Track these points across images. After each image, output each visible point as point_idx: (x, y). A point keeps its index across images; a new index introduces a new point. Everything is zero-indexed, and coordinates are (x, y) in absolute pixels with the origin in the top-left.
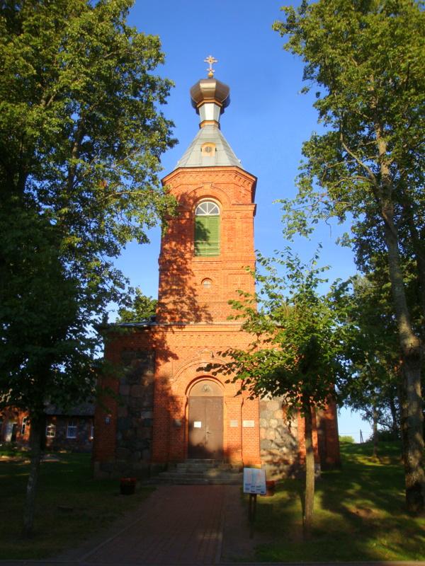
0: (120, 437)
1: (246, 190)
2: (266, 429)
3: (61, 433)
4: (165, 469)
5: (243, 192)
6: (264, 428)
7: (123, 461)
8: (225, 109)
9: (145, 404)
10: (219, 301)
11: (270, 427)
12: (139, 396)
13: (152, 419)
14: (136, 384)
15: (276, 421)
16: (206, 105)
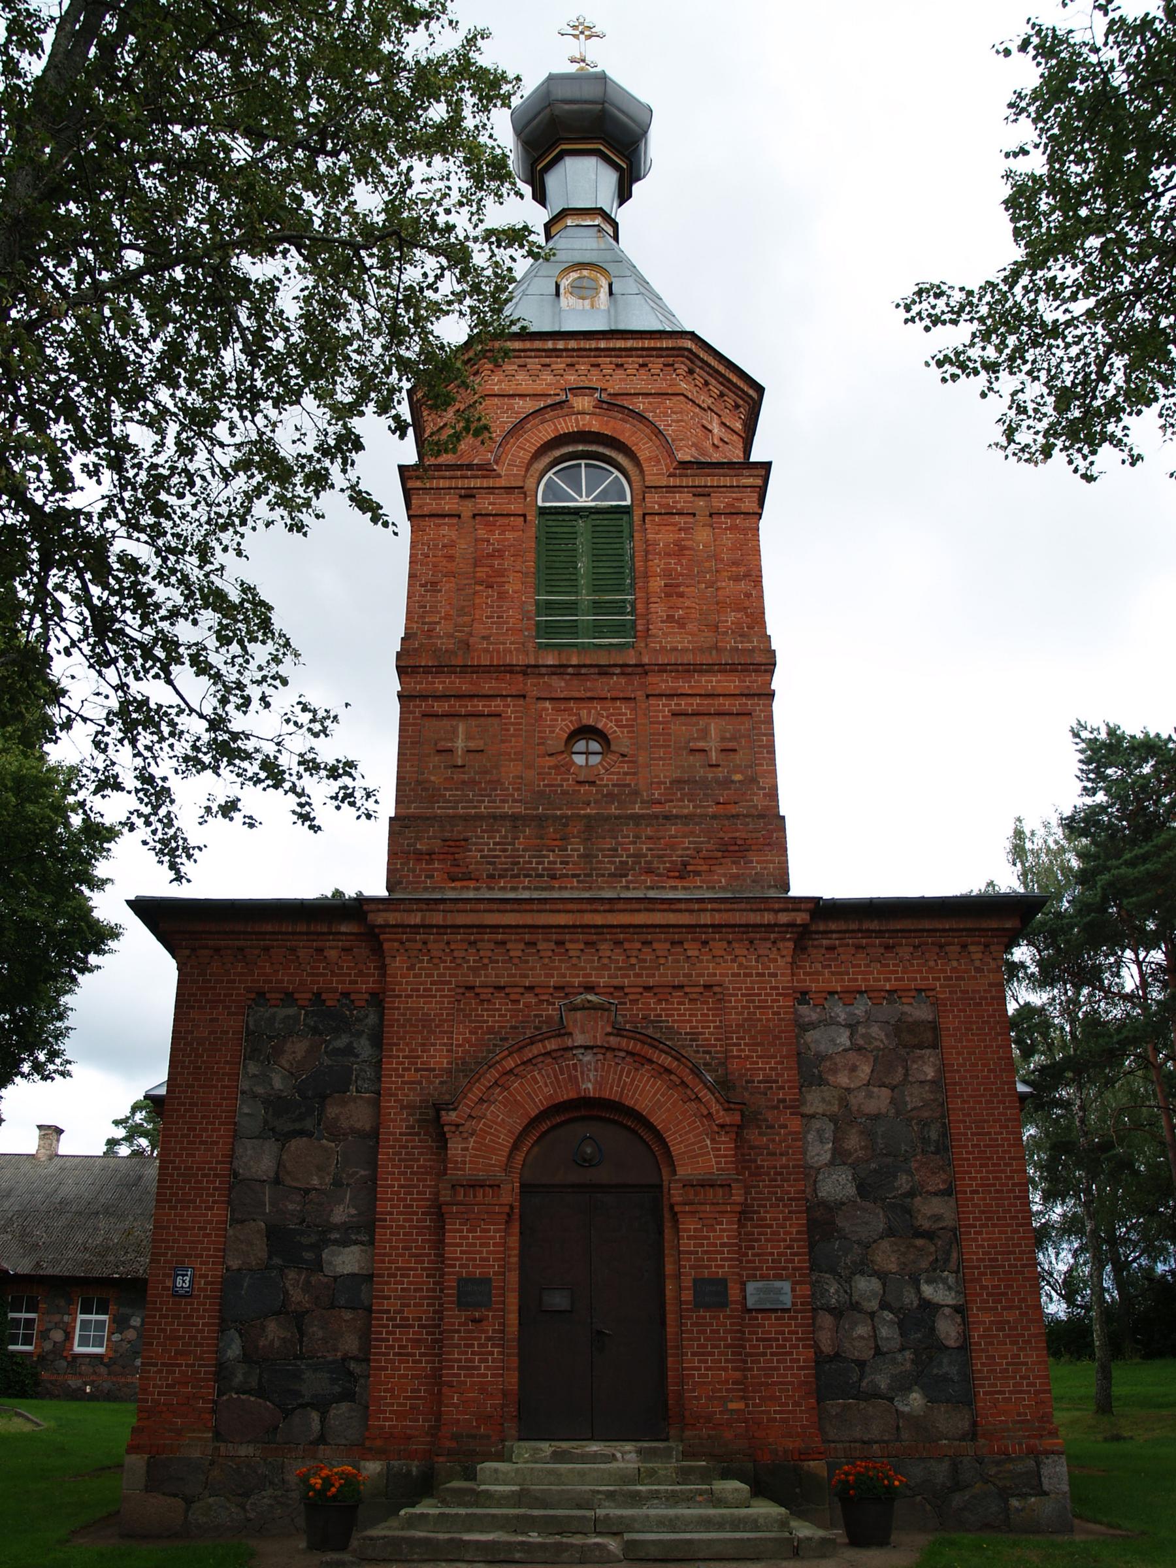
0: (234, 1351)
1: (723, 424)
2: (837, 1313)
3: (58, 1335)
4: (424, 1486)
5: (716, 429)
6: (830, 1310)
7: (245, 1450)
8: (636, 187)
9: (340, 1214)
10: (637, 809)
11: (855, 1307)
12: (315, 1182)
13: (369, 1278)
14: (301, 1133)
15: (875, 1284)
16: (570, 163)
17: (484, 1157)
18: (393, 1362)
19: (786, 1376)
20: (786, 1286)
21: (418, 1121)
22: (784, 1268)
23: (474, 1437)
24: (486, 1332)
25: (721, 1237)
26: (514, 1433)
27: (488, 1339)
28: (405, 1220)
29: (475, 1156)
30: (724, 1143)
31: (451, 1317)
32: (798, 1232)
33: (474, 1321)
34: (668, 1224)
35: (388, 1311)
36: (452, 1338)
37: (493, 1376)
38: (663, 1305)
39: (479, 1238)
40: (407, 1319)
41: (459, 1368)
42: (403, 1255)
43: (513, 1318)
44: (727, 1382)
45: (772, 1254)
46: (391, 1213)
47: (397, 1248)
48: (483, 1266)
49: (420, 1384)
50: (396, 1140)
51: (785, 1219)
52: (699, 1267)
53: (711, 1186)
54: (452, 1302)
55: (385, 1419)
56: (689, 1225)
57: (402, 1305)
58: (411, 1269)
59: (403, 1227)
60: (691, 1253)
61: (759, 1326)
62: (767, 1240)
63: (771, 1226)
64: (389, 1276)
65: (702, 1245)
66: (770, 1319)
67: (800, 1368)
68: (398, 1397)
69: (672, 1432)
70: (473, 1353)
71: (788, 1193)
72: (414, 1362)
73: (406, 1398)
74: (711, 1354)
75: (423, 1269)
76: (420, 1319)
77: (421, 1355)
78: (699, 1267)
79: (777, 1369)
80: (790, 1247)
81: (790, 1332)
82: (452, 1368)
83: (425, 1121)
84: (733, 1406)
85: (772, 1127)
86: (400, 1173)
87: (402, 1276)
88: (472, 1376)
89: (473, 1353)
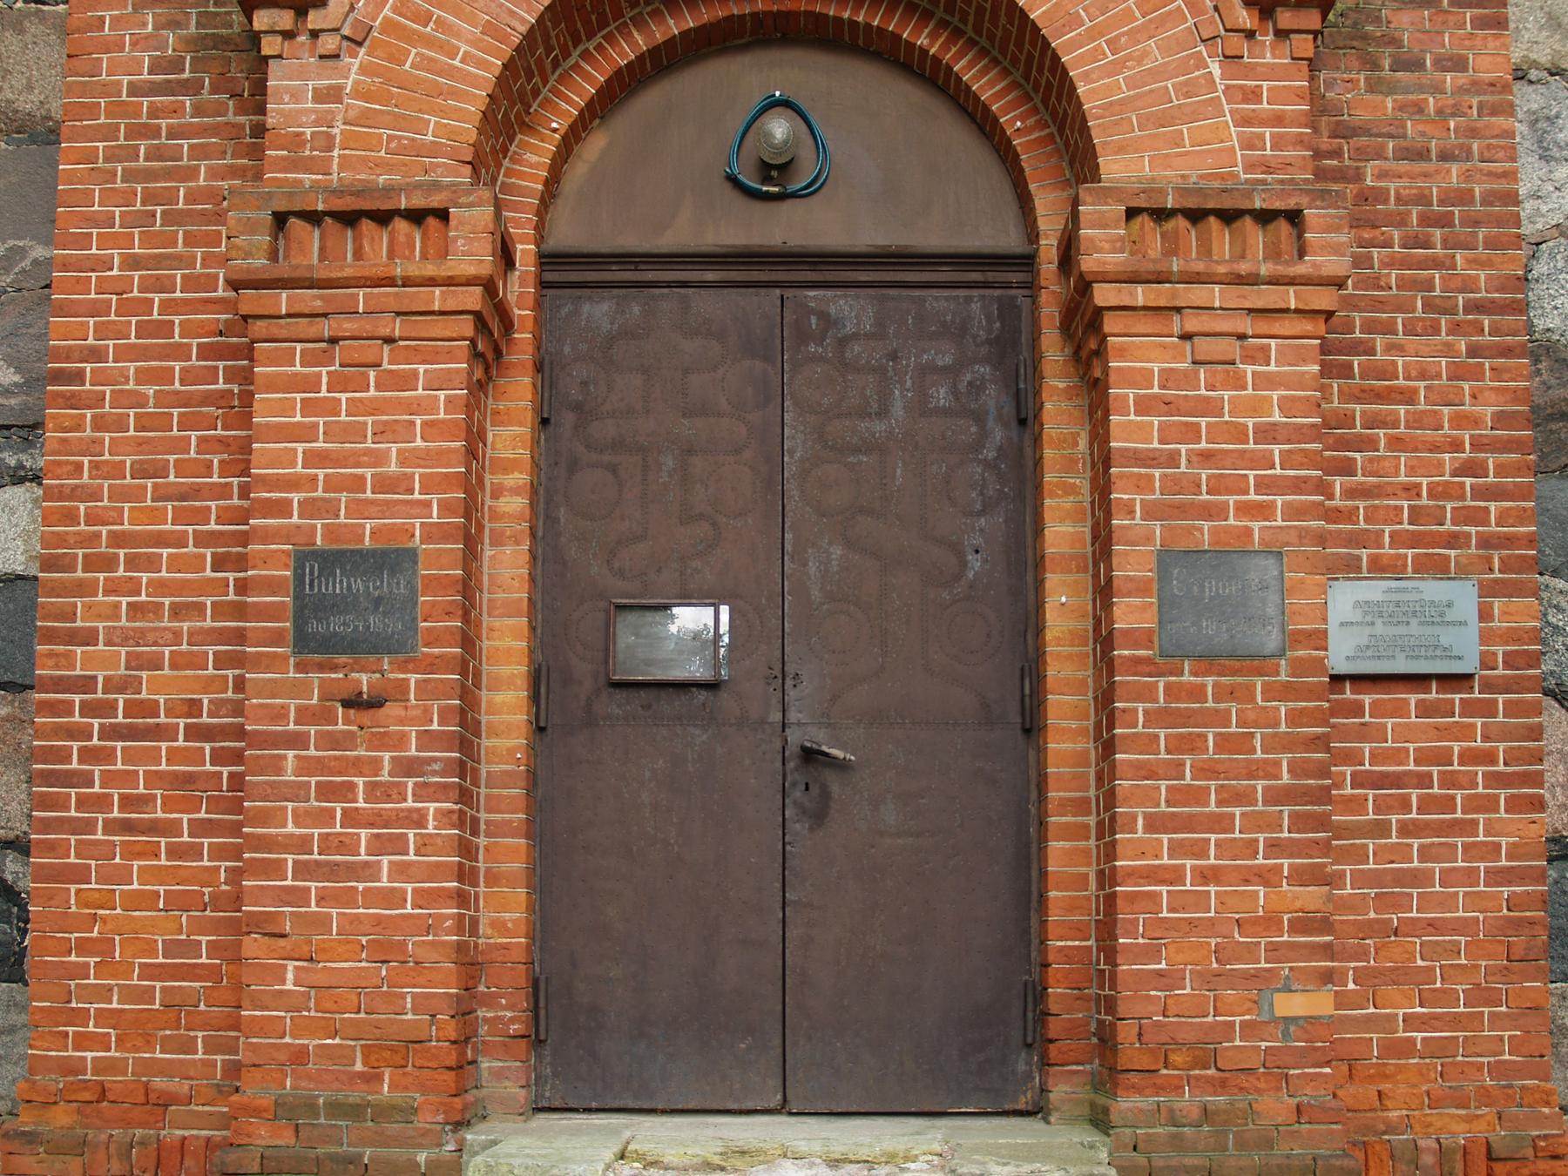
17: (398, 122)
18: (107, 851)
19: (1448, 902)
20: (1463, 596)
21: (195, 44)
22: (1453, 540)
23: (355, 1111)
24: (401, 741)
25: (1257, 407)
26: (515, 1090)
27: (408, 767)
28: (144, 377)
29: (365, 118)
30: (1271, 73)
31: (274, 689)
32: (1501, 420)
33: (353, 702)
34: (1056, 382)
35: (87, 684)
36: (277, 766)
37: (422, 898)
38: (1031, 671)
39: (374, 408)
40: (151, 709)
41: (302, 870)
42: (136, 494)
43: (506, 706)
44: (1271, 922)
45: (1412, 490)
46: (97, 355)
47: (117, 470)
48: (387, 509)
49: (199, 927)
50: (117, 109)
51: (1457, 374)
52: (1182, 510)
53: (1229, 217)
54: (276, 638)
55: (83, 1041)
56: (1141, 360)
57: (135, 662)
58: (161, 540)
59: (139, 400)
60: (1149, 459)
61: (1364, 733)
62: (1396, 443)
63: (1409, 397)
64: (91, 564)
65: (1192, 433)
66: (1400, 710)
67: (1499, 877)
68: (125, 970)
69: (1059, 1091)
70: (351, 818)
71: (1468, 286)
72: (174, 852)
73: (149, 972)
74: (1221, 823)
75: (203, 540)
76: (193, 708)
77: (198, 828)
78: (1182, 510)
79: (1418, 878)
80: (1471, 469)
81: (1469, 757)
82: (276, 869)
83: (220, 42)
84: (1291, 1005)
85: (1418, 65)
86: (129, 220)
87: (132, 563)
88: (348, 898)
89: (351, 818)
